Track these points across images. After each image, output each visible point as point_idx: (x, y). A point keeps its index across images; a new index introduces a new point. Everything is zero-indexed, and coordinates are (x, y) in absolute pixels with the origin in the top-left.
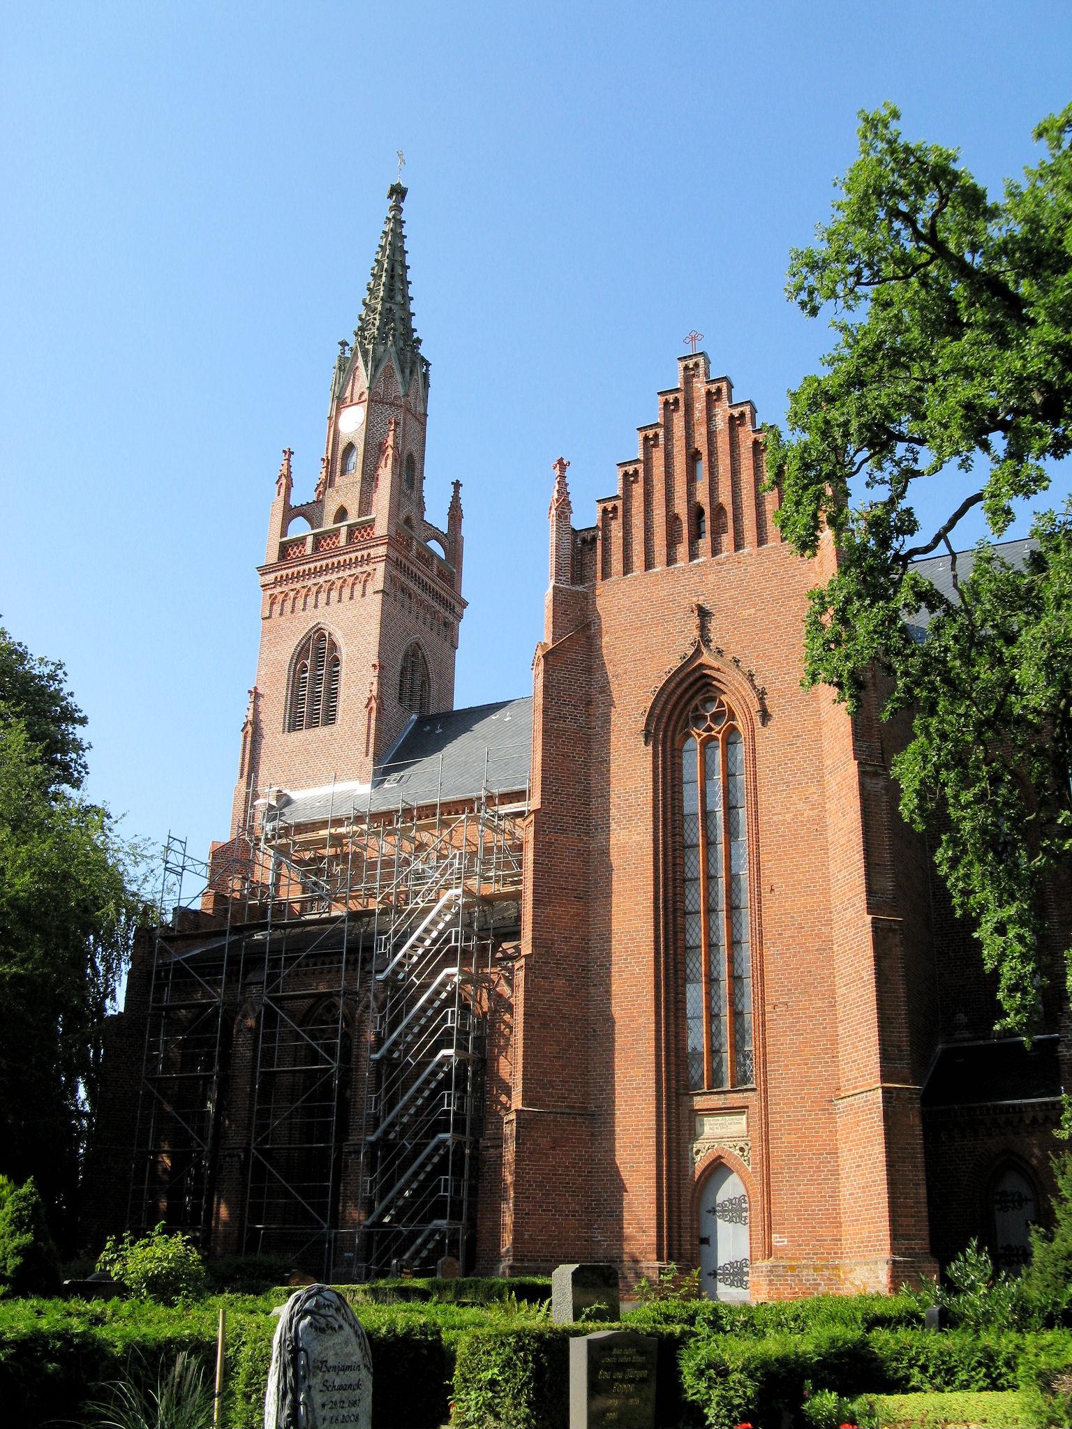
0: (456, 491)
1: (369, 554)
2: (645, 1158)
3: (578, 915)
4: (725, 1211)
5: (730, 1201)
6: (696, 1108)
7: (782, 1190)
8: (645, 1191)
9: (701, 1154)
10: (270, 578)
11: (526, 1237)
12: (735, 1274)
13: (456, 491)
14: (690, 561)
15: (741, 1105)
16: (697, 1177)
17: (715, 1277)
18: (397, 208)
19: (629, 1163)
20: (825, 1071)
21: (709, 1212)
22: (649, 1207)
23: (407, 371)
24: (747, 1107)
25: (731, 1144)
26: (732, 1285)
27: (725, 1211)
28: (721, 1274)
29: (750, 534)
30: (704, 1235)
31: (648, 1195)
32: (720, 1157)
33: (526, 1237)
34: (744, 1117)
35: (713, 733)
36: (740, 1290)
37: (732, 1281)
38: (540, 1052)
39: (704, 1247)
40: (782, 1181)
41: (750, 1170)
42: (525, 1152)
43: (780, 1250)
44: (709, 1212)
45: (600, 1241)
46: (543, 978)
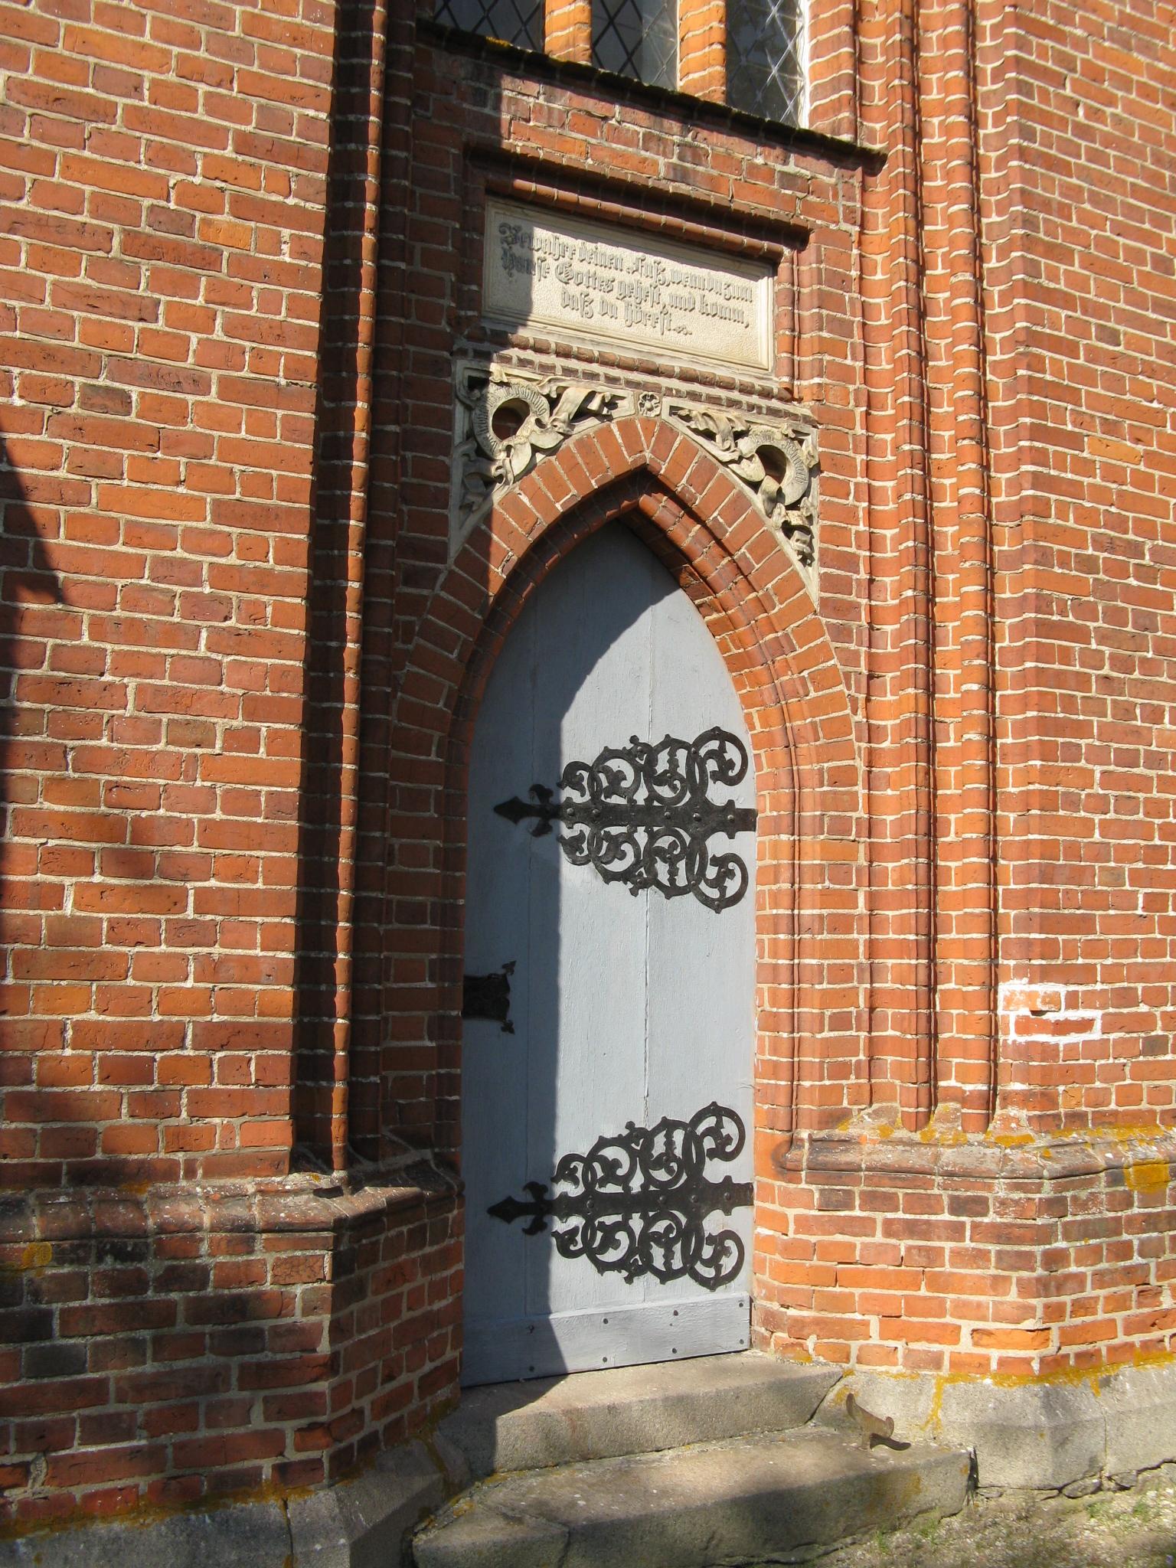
2: (230, 357)
4: (615, 815)
5: (641, 754)
6: (516, 144)
7: (1082, 730)
8: (216, 608)
9: (528, 430)
12: (650, 1202)
15: (773, 211)
16: (498, 573)
17: (539, 1226)
19: (85, 363)
21: (513, 810)
22: (244, 740)
24: (798, 237)
26: (633, 1267)
27: (615, 815)
28: (569, 1206)
30: (480, 962)
31: (236, 642)
32: (644, 478)
34: (763, 289)
36: (685, 1292)
37: (641, 1245)
39: (480, 1033)
40: (1083, 681)
41: (814, 591)
43: (1068, 1075)
44: (513, 810)
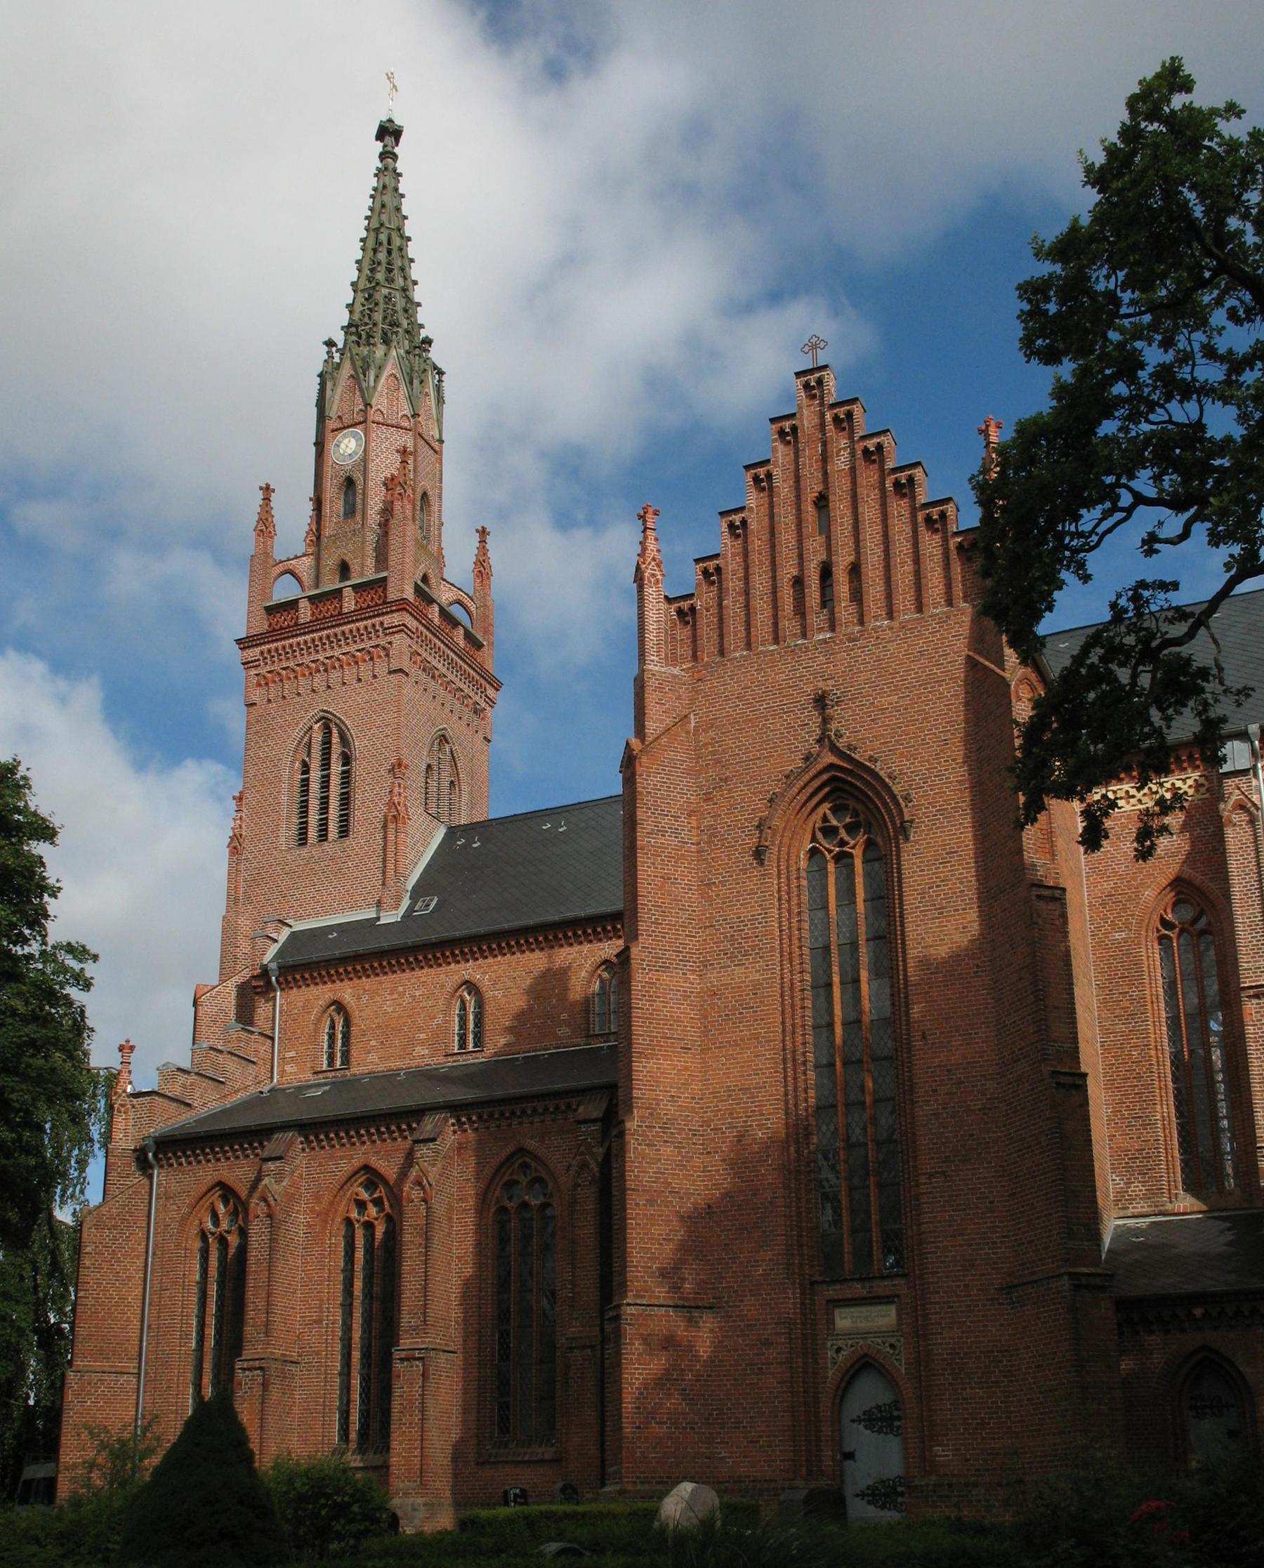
0: (267, 499)
1: (382, 623)
3: (686, 1069)
10: (254, 653)
11: (638, 1454)
13: (267, 499)
14: (385, 579)
18: (388, 155)
20: (994, 1253)
23: (416, 382)
25: (879, 1340)
26: (883, 1507)
29: (904, 598)
33: (638, 1454)
35: (846, 849)
38: (647, 1234)
41: (903, 1371)
42: (634, 1354)
45: (725, 1457)
46: (647, 1145)
